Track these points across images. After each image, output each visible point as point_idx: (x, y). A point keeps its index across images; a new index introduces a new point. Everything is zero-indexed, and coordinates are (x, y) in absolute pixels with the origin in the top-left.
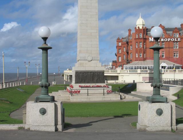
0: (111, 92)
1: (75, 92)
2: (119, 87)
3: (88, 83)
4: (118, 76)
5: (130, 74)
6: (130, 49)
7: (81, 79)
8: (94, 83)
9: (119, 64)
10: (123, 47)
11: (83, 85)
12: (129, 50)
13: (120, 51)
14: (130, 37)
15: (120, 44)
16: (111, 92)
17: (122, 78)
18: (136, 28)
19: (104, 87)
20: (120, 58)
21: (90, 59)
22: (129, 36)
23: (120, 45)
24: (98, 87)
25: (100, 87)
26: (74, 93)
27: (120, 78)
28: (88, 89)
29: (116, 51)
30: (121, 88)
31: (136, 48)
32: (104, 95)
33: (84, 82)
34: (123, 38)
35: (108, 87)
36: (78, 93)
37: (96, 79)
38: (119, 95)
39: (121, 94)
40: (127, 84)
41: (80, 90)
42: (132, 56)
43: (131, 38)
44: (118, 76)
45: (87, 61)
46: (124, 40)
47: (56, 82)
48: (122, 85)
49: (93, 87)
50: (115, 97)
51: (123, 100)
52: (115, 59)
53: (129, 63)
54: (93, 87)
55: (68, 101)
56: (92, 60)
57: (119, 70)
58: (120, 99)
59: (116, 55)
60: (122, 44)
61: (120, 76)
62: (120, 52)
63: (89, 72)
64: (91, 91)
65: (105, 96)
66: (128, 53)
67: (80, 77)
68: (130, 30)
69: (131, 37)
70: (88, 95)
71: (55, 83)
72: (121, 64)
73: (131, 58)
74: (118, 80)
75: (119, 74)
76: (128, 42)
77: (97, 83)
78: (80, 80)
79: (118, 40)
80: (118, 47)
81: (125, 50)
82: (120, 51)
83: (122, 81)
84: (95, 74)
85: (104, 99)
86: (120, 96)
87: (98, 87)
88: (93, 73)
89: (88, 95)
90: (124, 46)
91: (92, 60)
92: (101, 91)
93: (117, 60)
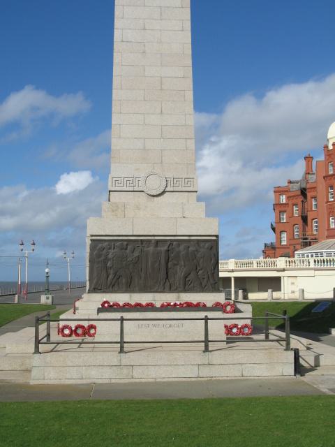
0: (246, 330)
1: (80, 331)
2: (285, 313)
3: (145, 289)
4: (278, 279)
5: (316, 272)
6: (311, 208)
7: (111, 272)
8: (171, 289)
9: (282, 251)
10: (290, 205)
11: (121, 298)
12: (309, 210)
13: (285, 217)
14: (310, 176)
15: (283, 199)
16: (246, 330)
17: (293, 283)
18: (326, 147)
19: (217, 307)
20: (284, 236)
21: (155, 185)
22: (309, 174)
23: (284, 202)
24: (189, 306)
25: (199, 307)
26: (77, 335)
27: (285, 283)
28: (122, 320)
29: (271, 217)
30: (291, 313)
31: (328, 202)
32: (206, 350)
33: (129, 288)
34: (290, 182)
35: (236, 311)
36: (84, 334)
37: (180, 271)
38: (288, 348)
39: (298, 342)
40: (313, 301)
41: (92, 323)
42: (317, 226)
43: (312, 178)
44: (278, 279)
45: (142, 198)
46: (296, 187)
47: (50, 296)
48: (294, 304)
49: (166, 307)
50: (265, 364)
51: (308, 377)
52: (271, 238)
53: (310, 245)
54: (166, 307)
55: (20, 379)
56: (164, 192)
57: (281, 262)
58: (293, 373)
59: (274, 229)
60: (288, 198)
61: (286, 278)
62: (285, 221)
63: (150, 241)
64: (135, 330)
65: (216, 357)
66: (305, 219)
67: (109, 264)
68: (308, 159)
69: (315, 177)
70: (122, 347)
71: (48, 298)
72: (287, 251)
73: (315, 233)
74: (279, 289)
75: (284, 270)
76: (305, 189)
77: (185, 291)
78: (111, 277)
79: (277, 189)
80: (277, 206)
81: (296, 211)
82: (284, 218)
83: (293, 292)
84: (179, 252)
85: (206, 373)
86: (292, 354)
87: (189, 306)
88: (166, 248)
89: (122, 347)
90: (295, 201)
91: (164, 192)
92: (192, 327)
93: (277, 242)
